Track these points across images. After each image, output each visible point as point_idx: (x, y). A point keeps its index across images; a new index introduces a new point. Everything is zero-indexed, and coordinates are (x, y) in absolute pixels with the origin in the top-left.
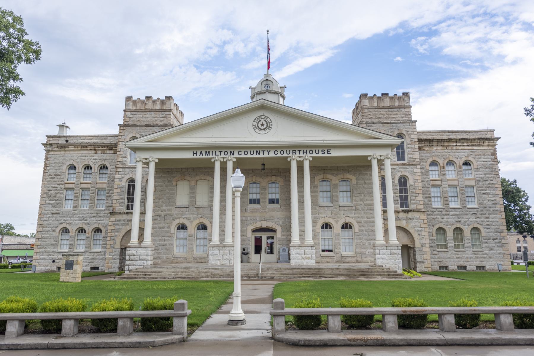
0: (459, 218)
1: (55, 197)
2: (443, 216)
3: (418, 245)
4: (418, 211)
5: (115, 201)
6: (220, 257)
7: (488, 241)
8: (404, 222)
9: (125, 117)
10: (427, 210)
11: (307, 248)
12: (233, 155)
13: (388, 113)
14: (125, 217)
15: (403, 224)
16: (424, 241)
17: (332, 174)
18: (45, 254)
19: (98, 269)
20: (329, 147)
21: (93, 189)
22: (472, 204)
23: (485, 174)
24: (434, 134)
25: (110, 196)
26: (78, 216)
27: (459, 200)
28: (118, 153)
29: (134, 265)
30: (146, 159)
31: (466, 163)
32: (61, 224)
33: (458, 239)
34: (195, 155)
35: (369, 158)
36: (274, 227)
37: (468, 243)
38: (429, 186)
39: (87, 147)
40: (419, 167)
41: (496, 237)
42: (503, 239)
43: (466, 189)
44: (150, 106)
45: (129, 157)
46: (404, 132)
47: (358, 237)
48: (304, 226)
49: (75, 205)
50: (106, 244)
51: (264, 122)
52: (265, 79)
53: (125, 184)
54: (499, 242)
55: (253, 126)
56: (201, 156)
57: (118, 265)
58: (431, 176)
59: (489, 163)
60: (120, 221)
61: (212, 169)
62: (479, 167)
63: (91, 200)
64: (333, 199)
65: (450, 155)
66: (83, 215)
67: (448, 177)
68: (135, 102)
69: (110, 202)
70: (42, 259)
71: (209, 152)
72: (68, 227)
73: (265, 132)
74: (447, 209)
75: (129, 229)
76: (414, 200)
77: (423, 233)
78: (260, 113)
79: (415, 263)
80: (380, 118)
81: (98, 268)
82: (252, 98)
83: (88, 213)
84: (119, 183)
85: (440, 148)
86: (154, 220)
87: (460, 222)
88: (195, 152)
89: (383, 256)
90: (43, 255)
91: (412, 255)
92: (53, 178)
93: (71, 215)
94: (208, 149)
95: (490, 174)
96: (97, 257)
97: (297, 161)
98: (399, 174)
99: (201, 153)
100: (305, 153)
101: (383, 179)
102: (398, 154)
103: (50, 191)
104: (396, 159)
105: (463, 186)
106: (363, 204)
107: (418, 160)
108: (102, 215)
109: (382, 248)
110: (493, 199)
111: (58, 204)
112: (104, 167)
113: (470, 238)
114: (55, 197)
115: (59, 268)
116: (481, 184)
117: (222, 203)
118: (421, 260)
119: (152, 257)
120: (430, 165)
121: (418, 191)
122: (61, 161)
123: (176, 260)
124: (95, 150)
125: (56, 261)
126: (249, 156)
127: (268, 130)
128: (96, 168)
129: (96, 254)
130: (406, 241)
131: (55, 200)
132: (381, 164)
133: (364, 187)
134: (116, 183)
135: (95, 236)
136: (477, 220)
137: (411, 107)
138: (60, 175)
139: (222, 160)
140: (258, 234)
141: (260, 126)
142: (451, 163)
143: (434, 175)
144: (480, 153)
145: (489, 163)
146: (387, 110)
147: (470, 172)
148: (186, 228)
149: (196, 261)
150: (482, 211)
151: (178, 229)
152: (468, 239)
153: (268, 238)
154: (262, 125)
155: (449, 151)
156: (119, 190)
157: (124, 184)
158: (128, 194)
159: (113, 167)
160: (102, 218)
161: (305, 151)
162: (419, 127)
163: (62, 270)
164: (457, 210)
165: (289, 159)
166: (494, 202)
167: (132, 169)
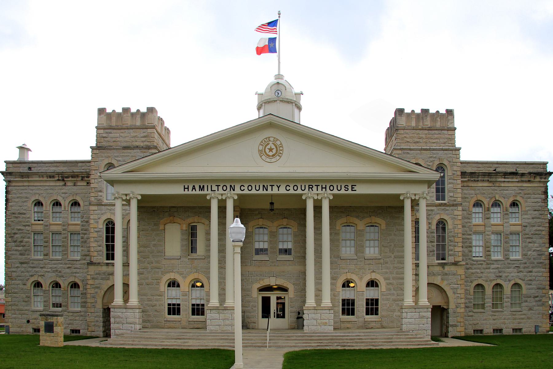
0: (500, 272)
1: (21, 242)
2: (483, 271)
3: (452, 306)
4: (455, 264)
5: (92, 249)
6: (221, 322)
7: (529, 299)
8: (439, 278)
9: (99, 137)
10: (469, 262)
11: (324, 311)
12: (234, 190)
13: (428, 136)
14: (104, 268)
15: (437, 280)
16: (459, 301)
17: (357, 217)
18: (17, 312)
19: (79, 333)
20: (353, 182)
21: (64, 232)
22: (516, 256)
23: (533, 218)
24: (480, 165)
25: (85, 242)
26: (50, 266)
27: (502, 251)
28: (92, 185)
29: (120, 329)
30: (126, 195)
31: (514, 204)
32: (32, 276)
33: (497, 298)
34: (186, 190)
35: (402, 198)
36: (285, 285)
37: (507, 302)
38: (471, 233)
39: (53, 177)
40: (460, 208)
41: (537, 295)
42: (544, 296)
43: (510, 237)
44: (129, 122)
45: (105, 190)
46: (446, 163)
47: (385, 297)
48: (321, 284)
49: (45, 253)
50: (85, 302)
51: (273, 147)
52: (276, 81)
53: (102, 227)
54: (540, 301)
55: (259, 151)
56: (194, 192)
57: (101, 329)
58: (474, 220)
59: (539, 204)
60: (99, 274)
61: (208, 209)
62: (528, 208)
63: (63, 246)
64: (360, 249)
65: (497, 193)
66: (55, 266)
67: (493, 221)
68: (110, 116)
69: (86, 249)
70: (15, 318)
71: (203, 186)
72: (41, 280)
73: (273, 160)
74: (488, 261)
75: (111, 285)
76: (452, 250)
77: (459, 291)
78: (270, 133)
79: (447, 327)
80: (418, 142)
81: (79, 331)
82: (259, 108)
83: (61, 264)
84: (95, 225)
85: (486, 184)
86: (139, 274)
87: (501, 277)
88: (186, 187)
89: (410, 320)
90: (15, 314)
91: (445, 318)
92: (16, 218)
93: (42, 266)
94: (203, 182)
95: (539, 218)
96: (77, 318)
97: (314, 200)
98: (437, 217)
99: (194, 188)
100: (324, 190)
101: (417, 222)
102: (437, 191)
103: (15, 234)
104: (434, 198)
105: (508, 233)
106: (393, 257)
107: (459, 200)
108: (78, 266)
109: (411, 310)
110: (538, 249)
111: (26, 251)
112: (75, 204)
113: (509, 296)
114: (21, 242)
115: (37, 330)
116: (527, 229)
117: (221, 254)
118: (454, 323)
119: (141, 320)
120: (474, 206)
121: (457, 240)
122: (25, 195)
123: (168, 324)
124: (63, 180)
125: (31, 321)
126: (254, 192)
127: (278, 158)
128: (67, 205)
129: (75, 314)
130: (439, 301)
131: (23, 246)
132: (415, 204)
133: (395, 235)
134: (92, 226)
135: (72, 292)
136: (519, 274)
137: (455, 129)
138: (25, 214)
139: (220, 198)
140: (266, 294)
141: (267, 151)
142: (496, 204)
143: (477, 219)
144: (530, 192)
145: (539, 204)
146: (426, 132)
147: (517, 215)
148: (178, 286)
149: (192, 326)
150: (526, 263)
151: (169, 286)
152: (508, 298)
153: (278, 298)
154: (271, 150)
155: (496, 188)
156: (95, 235)
157: (101, 227)
158: (107, 241)
159: (87, 203)
160: (78, 270)
161: (324, 186)
162: (464, 156)
163: (42, 332)
164: (499, 262)
165: (304, 198)
166: (539, 253)
167: (109, 207)
